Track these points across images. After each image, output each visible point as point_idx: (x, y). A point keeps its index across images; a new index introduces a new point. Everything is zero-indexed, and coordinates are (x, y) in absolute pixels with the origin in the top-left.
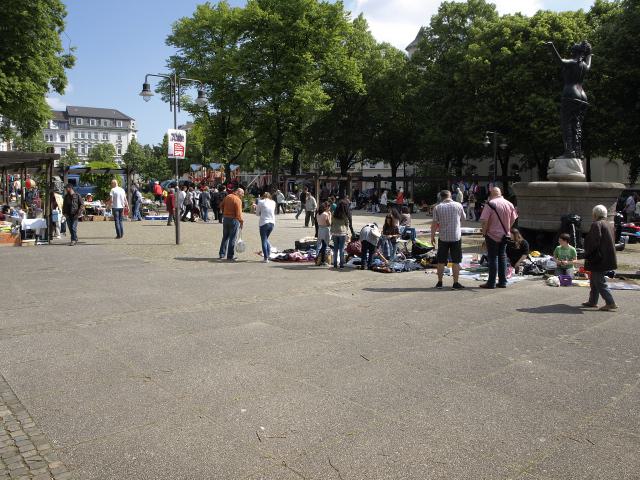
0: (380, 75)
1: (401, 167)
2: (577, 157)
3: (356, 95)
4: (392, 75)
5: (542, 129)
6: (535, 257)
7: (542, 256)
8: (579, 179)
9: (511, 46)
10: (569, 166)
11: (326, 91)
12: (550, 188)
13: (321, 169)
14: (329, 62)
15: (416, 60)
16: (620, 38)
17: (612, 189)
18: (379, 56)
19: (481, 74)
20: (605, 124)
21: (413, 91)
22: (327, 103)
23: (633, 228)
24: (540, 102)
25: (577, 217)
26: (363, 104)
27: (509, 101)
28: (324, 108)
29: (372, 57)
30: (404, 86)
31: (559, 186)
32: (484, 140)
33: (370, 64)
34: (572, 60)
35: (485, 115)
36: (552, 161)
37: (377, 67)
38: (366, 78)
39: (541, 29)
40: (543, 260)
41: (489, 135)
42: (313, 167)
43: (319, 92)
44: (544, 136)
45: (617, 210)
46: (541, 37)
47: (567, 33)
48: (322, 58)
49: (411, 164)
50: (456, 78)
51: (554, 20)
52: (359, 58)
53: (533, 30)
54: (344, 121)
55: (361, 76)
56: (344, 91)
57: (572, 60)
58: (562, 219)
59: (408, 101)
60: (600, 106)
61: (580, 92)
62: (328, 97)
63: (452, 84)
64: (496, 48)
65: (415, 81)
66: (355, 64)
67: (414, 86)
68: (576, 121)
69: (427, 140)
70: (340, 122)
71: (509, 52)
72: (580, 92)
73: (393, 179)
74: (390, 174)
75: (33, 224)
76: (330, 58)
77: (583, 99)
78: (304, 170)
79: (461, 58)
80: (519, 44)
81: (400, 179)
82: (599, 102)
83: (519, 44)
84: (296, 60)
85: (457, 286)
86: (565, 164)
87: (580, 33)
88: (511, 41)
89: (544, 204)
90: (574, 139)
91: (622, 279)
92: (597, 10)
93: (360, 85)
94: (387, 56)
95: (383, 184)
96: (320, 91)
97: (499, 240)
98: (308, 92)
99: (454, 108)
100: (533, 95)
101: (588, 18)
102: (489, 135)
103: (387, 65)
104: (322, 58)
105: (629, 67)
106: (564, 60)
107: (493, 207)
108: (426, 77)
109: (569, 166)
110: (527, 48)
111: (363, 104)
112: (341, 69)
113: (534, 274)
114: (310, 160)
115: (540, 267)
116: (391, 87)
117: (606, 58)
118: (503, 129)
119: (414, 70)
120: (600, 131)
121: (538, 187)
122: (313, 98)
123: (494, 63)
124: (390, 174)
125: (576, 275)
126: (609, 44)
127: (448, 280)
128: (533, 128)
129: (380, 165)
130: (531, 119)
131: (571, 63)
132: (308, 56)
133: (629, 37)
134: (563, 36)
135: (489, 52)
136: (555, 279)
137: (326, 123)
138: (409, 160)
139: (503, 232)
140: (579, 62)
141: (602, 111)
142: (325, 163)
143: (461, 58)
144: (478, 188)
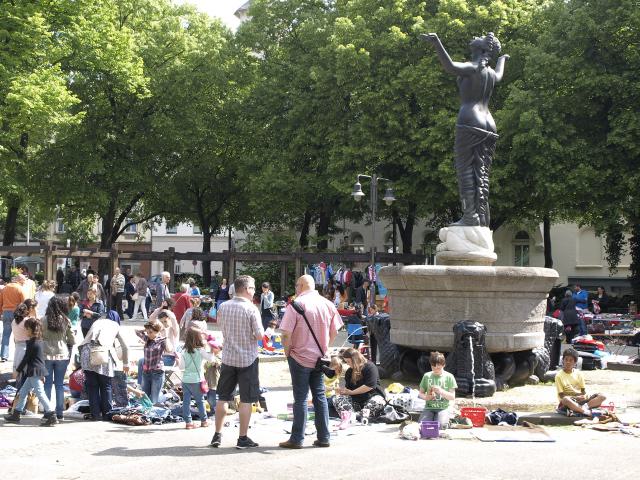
0: (178, 62)
1: (224, 232)
2: (482, 224)
3: (133, 98)
4: (199, 64)
6: (395, 392)
7: (406, 391)
8: (486, 262)
9: (406, 25)
10: (469, 239)
11: (73, 88)
12: (435, 276)
13: (70, 235)
14: (80, 32)
15: (245, 37)
16: (577, 25)
17: (534, 278)
18: (176, 28)
19: (354, 73)
21: (241, 94)
22: (75, 110)
23: (590, 344)
25: (478, 326)
26: (146, 115)
27: (402, 122)
28: (66, 118)
29: (165, 28)
30: (222, 84)
31: (449, 273)
32: (356, 189)
33: (160, 40)
35: (360, 146)
37: (173, 48)
38: (151, 67)
40: (406, 397)
41: (362, 180)
42: (54, 229)
43: (58, 88)
45: (550, 311)
47: (498, 11)
48: (67, 23)
49: (241, 228)
50: (313, 74)
52: (138, 28)
54: (109, 144)
55: (141, 63)
56: (110, 89)
58: (455, 329)
59: (231, 113)
60: (551, 135)
61: (483, 115)
62: (74, 99)
63: (306, 87)
64: (381, 28)
65: (242, 77)
66: (132, 41)
67: (242, 84)
68: (476, 164)
69: (262, 186)
70: (100, 147)
71: (404, 36)
72: (483, 115)
73: (206, 257)
74: (198, 247)
75: (17, 343)
76: (80, 28)
77: (489, 128)
78: (35, 235)
79: (323, 39)
80: (419, 22)
81: (217, 257)
82: (549, 130)
83: (419, 22)
84: (13, 27)
85: (245, 443)
86: (462, 235)
87: (519, 9)
88: (406, 17)
89: (427, 303)
90: (477, 193)
91: (526, 425)
93: (137, 78)
94: (191, 28)
95: (186, 266)
96: (58, 85)
97: (312, 366)
98: (37, 89)
99: (309, 128)
102: (362, 180)
103: (192, 45)
104: (67, 23)
105: (593, 72)
106: (457, 64)
107: (300, 310)
108: (264, 69)
109: (469, 239)
111: (146, 115)
112: (103, 48)
113: (389, 422)
114: (46, 216)
115: (399, 409)
116: (197, 86)
117: (557, 55)
118: (392, 171)
119: (242, 55)
120: (554, 178)
121: (417, 271)
122: (46, 100)
123: (378, 54)
124: (198, 247)
125: (453, 421)
126: (561, 35)
127: (230, 437)
128: (444, 172)
129: (186, 229)
130: (440, 155)
131: (468, 69)
132: (38, 19)
133: (591, 23)
134: (491, 14)
135: (368, 33)
136: (414, 428)
137: (73, 148)
138: (238, 219)
139: (316, 351)
140: (481, 68)
141: (554, 144)
142: (77, 223)
143: (323, 39)
144: (349, 275)
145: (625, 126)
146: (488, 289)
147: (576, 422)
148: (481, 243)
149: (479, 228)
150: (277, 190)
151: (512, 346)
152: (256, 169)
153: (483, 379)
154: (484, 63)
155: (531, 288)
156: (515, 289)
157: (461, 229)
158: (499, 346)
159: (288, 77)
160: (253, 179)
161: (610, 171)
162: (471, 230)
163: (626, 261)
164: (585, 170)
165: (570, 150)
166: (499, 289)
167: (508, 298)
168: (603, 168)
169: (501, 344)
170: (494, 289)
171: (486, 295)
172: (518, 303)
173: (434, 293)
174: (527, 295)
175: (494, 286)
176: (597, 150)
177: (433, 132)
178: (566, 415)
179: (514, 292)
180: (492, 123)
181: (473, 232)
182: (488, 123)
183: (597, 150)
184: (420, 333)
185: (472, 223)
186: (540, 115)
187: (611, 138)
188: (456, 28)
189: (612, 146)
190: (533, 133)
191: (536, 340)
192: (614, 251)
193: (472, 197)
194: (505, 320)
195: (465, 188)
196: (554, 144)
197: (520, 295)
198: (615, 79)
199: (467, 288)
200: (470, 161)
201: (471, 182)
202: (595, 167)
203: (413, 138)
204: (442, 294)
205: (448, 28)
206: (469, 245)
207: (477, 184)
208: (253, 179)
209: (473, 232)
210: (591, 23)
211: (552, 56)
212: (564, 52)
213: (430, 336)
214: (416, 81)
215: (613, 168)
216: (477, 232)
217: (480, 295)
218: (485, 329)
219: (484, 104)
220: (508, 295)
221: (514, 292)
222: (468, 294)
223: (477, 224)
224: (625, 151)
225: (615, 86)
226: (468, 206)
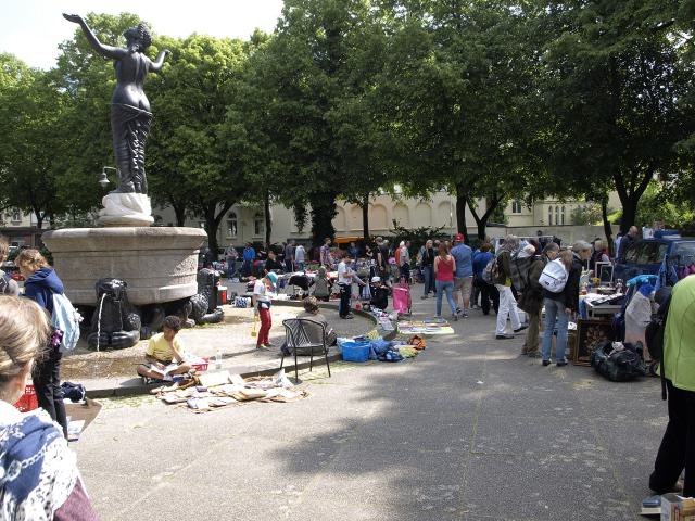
2: (138, 191)
5: (193, 168)
10: (125, 204)
17: (174, 236)
20: (259, 162)
24: (190, 136)
34: (433, 363)
36: (542, 279)
39: (191, 50)
44: (194, 176)
46: (191, 59)
47: (220, 59)
51: (208, 43)
53: (182, 51)
57: (433, 363)
60: (254, 141)
61: (480, 382)
68: (130, 138)
77: (141, 105)
86: (119, 201)
89: (76, 263)
90: (131, 165)
92: (256, 39)
100: (182, 127)
101: (246, 47)
109: (125, 204)
110: (174, 72)
120: (255, 170)
128: (182, 167)
133: (278, 66)
145: (301, 135)
146: (129, 248)
147: (153, 391)
148: (137, 208)
149: (134, 195)
150: (75, 185)
151: (158, 298)
152: (61, 172)
153: (123, 333)
154: (134, 48)
155: (174, 245)
156: (158, 247)
157: (117, 195)
158: (145, 298)
159: (83, 107)
160: (58, 178)
161: (292, 166)
162: (126, 196)
163: (309, 225)
164: (276, 165)
165: (266, 151)
166: (144, 247)
167: (152, 255)
168: (288, 163)
169: (147, 297)
170: (135, 248)
171: (129, 253)
172: (162, 260)
173: (82, 254)
174: (171, 251)
175: (135, 245)
176: (284, 152)
177: (175, 139)
178: (144, 386)
179: (157, 250)
180: (146, 103)
181: (128, 198)
182: (140, 102)
183: (284, 152)
184: (73, 291)
185: (127, 190)
186: (246, 127)
187: (293, 143)
188: (191, 70)
189: (295, 149)
190: (240, 140)
191: (187, 286)
192: (300, 219)
193: (126, 167)
194: (150, 276)
195: (120, 160)
196: (255, 147)
197: (164, 252)
198: (295, 103)
199: (110, 248)
200: (123, 137)
201: (126, 154)
202: (282, 163)
203: (164, 144)
204: (88, 254)
205: (185, 70)
206: (124, 210)
207: (131, 155)
208: (58, 178)
209: (128, 198)
210: (278, 66)
211: (253, 87)
212: (260, 85)
213: (81, 293)
214: (164, 106)
215: (294, 163)
216: (132, 198)
217: (123, 253)
218: (125, 285)
219: (137, 85)
220: (150, 253)
221: (157, 250)
222: (111, 253)
223: (132, 191)
224: (303, 152)
225: (294, 108)
226: (123, 175)
